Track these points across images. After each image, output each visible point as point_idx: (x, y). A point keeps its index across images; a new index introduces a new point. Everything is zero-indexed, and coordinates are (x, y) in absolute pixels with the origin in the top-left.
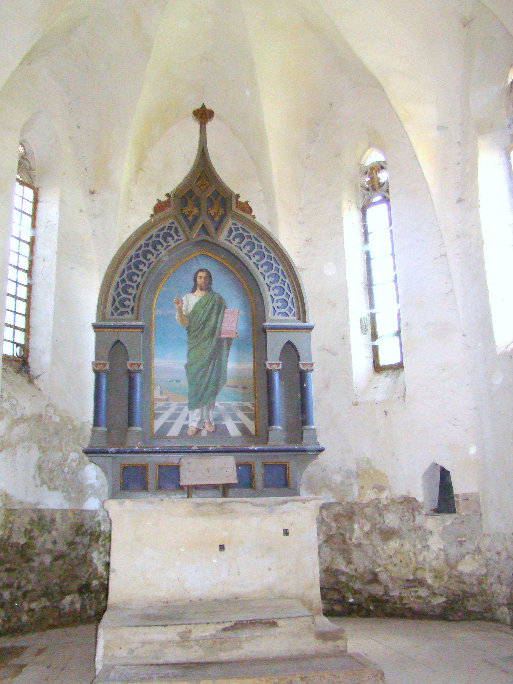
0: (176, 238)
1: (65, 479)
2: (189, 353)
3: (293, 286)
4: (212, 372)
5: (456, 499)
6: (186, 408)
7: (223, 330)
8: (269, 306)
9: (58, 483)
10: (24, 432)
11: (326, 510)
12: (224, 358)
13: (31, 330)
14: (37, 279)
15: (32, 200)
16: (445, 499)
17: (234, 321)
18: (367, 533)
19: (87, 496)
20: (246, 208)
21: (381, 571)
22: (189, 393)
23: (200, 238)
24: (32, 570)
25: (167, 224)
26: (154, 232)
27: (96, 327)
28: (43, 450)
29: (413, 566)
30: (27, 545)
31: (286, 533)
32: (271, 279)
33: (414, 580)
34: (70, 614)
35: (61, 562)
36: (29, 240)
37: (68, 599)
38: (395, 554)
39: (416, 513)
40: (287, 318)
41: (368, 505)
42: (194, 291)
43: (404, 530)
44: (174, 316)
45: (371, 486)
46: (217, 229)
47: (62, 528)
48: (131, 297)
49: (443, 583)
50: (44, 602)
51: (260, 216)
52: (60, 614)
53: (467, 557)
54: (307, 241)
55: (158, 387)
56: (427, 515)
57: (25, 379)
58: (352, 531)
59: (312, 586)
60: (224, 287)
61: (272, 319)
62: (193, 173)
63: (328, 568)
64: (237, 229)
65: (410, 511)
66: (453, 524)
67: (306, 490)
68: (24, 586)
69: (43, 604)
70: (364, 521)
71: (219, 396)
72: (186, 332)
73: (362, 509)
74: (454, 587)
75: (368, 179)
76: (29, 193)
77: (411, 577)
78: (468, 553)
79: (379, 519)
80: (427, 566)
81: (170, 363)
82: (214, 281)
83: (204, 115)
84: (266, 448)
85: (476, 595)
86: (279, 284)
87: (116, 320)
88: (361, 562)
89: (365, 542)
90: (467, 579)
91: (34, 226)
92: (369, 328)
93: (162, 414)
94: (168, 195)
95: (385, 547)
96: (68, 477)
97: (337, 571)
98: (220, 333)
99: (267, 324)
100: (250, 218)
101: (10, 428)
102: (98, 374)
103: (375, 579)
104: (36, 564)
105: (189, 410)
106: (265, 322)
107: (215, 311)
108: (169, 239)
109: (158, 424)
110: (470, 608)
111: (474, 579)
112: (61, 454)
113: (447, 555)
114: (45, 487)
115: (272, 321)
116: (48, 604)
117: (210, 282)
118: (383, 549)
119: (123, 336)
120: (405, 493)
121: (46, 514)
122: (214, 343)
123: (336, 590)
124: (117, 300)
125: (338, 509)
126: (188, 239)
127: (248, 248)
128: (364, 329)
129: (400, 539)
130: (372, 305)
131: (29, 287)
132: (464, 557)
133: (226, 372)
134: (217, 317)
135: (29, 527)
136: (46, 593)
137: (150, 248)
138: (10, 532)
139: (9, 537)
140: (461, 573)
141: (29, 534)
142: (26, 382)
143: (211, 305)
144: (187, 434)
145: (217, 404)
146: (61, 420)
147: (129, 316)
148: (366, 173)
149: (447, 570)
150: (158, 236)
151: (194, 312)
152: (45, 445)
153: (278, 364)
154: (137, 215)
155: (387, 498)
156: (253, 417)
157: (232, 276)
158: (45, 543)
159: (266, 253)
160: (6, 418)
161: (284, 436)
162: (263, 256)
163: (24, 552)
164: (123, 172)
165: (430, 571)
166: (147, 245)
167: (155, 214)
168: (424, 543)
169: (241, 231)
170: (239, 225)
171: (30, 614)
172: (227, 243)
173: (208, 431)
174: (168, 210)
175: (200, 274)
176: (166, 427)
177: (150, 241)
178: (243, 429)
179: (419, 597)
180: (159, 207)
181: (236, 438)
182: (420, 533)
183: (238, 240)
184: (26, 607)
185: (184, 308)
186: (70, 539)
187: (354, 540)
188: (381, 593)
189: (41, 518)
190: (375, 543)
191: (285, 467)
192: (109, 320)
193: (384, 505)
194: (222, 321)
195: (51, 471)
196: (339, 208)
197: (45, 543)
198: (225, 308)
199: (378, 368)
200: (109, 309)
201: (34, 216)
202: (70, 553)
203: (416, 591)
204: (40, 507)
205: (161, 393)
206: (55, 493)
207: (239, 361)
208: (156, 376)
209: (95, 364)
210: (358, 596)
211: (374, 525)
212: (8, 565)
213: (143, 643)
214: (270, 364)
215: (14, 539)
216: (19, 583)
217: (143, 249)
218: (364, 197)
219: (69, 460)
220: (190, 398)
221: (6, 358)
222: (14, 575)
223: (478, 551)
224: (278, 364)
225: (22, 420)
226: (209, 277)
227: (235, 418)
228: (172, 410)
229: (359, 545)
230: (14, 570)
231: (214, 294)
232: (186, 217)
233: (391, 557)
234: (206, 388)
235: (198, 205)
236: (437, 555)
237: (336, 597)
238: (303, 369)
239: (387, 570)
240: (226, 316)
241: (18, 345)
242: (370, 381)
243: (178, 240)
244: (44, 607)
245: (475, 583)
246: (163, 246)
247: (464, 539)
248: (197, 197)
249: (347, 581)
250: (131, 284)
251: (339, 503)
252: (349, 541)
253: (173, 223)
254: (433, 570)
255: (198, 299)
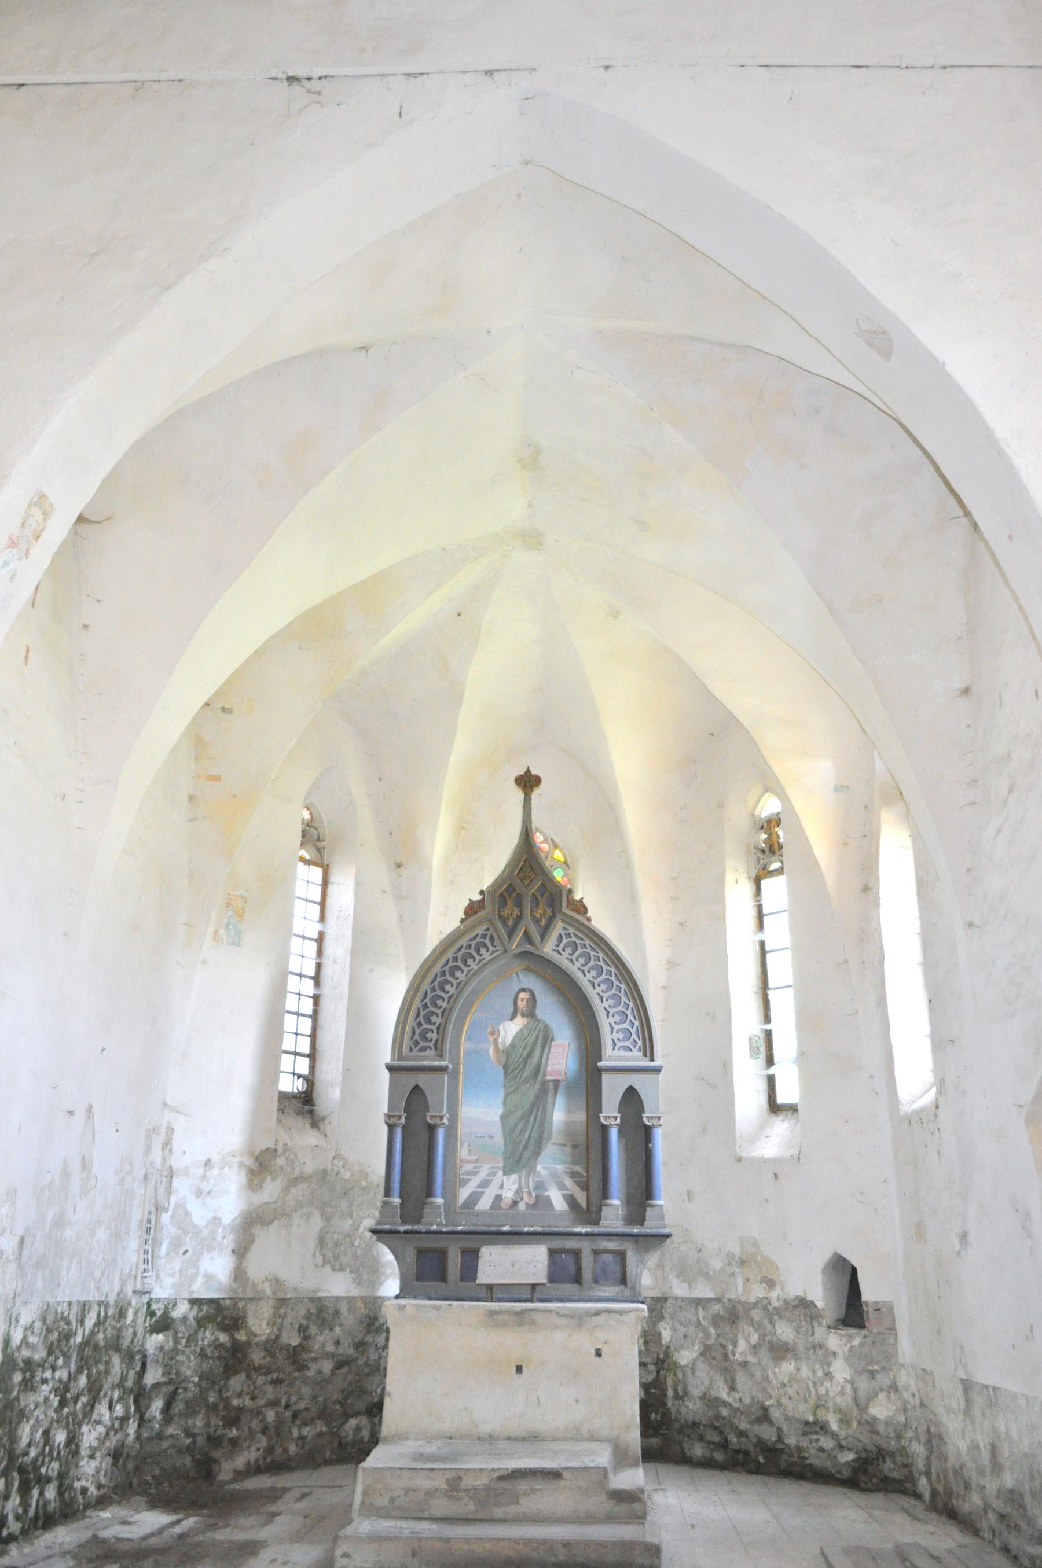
0: (491, 949)
1: (355, 1255)
2: (507, 1096)
3: (639, 1011)
4: (533, 1126)
5: (865, 1308)
6: (500, 1173)
7: (549, 1068)
8: (607, 1050)
9: (345, 1260)
10: (303, 1195)
11: (704, 1308)
12: (549, 1106)
13: (318, 1056)
14: (327, 990)
15: (320, 882)
16: (853, 1311)
17: (562, 1058)
18: (754, 1347)
19: (383, 1278)
20: (581, 908)
21: (772, 1405)
22: (505, 1153)
23: (521, 949)
24: (305, 1381)
25: (481, 930)
26: (464, 941)
27: (390, 1068)
28: (327, 1218)
29: (812, 1401)
30: (301, 1347)
31: (598, 1353)
32: (611, 1002)
33: (815, 1423)
34: (354, 1443)
35: (344, 1370)
36: (316, 936)
37: (353, 1422)
38: (789, 1381)
39: (816, 1324)
40: (629, 1054)
41: (755, 1305)
42: (513, 1017)
43: (801, 1348)
44: (487, 1051)
45: (759, 1278)
46: (543, 936)
47: (349, 1320)
48: (434, 1028)
49: (850, 1432)
50: (320, 1427)
51: (600, 919)
52: (340, 1443)
53: (882, 1396)
54: (681, 924)
55: (466, 1144)
56: (829, 1327)
57: (307, 1123)
58: (735, 1344)
59: (628, 1427)
60: (552, 1013)
61: (611, 1055)
62: (511, 865)
63: (705, 1394)
64: (569, 936)
65: (809, 1319)
66: (861, 1345)
67: (678, 1276)
68: (295, 1403)
69: (318, 1429)
70: (751, 1329)
71: (541, 1158)
72: (502, 1072)
73: (747, 1312)
74: (865, 1438)
75: (764, 836)
76: (317, 873)
77: (811, 1419)
78: (882, 1390)
79: (769, 1327)
80: (831, 1404)
81: (479, 1113)
82: (538, 1003)
83: (528, 782)
84: (596, 1230)
85: (893, 1453)
86: (620, 1008)
87: (414, 1059)
88: (746, 1392)
89: (751, 1359)
90: (881, 1428)
91: (322, 918)
92: (763, 1049)
93: (470, 1180)
94: (482, 892)
95: (777, 1370)
96: (359, 1252)
97: (717, 1399)
98: (545, 1074)
99: (600, 1064)
100: (585, 922)
101: (286, 1190)
102: (391, 1128)
103: (764, 1416)
104: (310, 1373)
105: (504, 1174)
106: (601, 1060)
107: (539, 1044)
108: (483, 951)
109: (464, 1194)
110: (887, 1473)
111: (890, 1429)
112: (351, 1222)
113: (855, 1390)
114: (328, 1268)
115: (610, 1059)
116: (324, 1429)
117: (534, 1007)
118: (774, 1373)
119: (423, 1080)
120: (801, 1294)
121: (328, 1304)
122: (537, 1087)
123: (716, 1428)
124: (418, 1031)
125: (717, 1308)
126: (506, 951)
127: (582, 961)
128: (754, 1052)
129: (797, 1359)
130: (767, 1019)
131: (316, 999)
132: (876, 1395)
133: (551, 1124)
134: (542, 1052)
135: (304, 1322)
136: (324, 1414)
137: (460, 964)
138: (280, 1329)
139: (278, 1337)
140: (875, 1419)
141: (304, 1332)
142: (308, 1126)
143: (534, 1036)
144: (501, 1208)
145: (539, 1168)
146: (352, 1175)
147: (431, 1053)
148: (762, 828)
149: (855, 1412)
150: (469, 947)
151: (513, 1045)
152: (329, 1210)
153: (616, 1118)
154: (442, 918)
155: (778, 1299)
156: (585, 1187)
157: (562, 999)
158: (323, 1345)
159: (605, 967)
160: (280, 1178)
161: (620, 1212)
162: (600, 972)
163: (297, 1357)
164: (439, 842)
165: (835, 1412)
166: (456, 959)
167: (466, 918)
168: (826, 1368)
169: (574, 939)
170: (571, 930)
171: (300, 1442)
172: (556, 954)
173: (527, 1204)
174: (482, 913)
175: (522, 995)
176: (474, 1198)
177: (460, 954)
178: (571, 1201)
179: (822, 1450)
180: (472, 909)
181: (561, 1215)
182: (820, 1353)
183: (569, 950)
184: (295, 1434)
185: (500, 1040)
186: (360, 1337)
187: (737, 1356)
188: (774, 1439)
189: (321, 1309)
190: (764, 1363)
191: (622, 1255)
192: (406, 1059)
193: (775, 1309)
194: (548, 1058)
195: (337, 1245)
196: (721, 881)
197: (323, 1345)
198: (553, 1040)
199: (774, 1107)
200: (407, 1043)
201: (323, 904)
202: (357, 1358)
203: (817, 1440)
204: (320, 1294)
205: (470, 1151)
206: (341, 1275)
207: (568, 1111)
208: (462, 1130)
209: (389, 1116)
210: (744, 1440)
211: (762, 1337)
212: (275, 1375)
213: (407, 1491)
214: (606, 1118)
215: (285, 1339)
216: (288, 1399)
217: (450, 964)
218: (759, 862)
219: (361, 1229)
220: (506, 1159)
221: (284, 1096)
222: (284, 1388)
223: (894, 1387)
224: (616, 1118)
225: (301, 1179)
226: (533, 999)
227: (562, 1187)
228: (482, 1177)
229: (745, 1364)
230: (282, 1382)
231: (538, 1021)
232: (504, 921)
233: (785, 1385)
234: (526, 1147)
235: (519, 904)
236: (842, 1387)
237: (716, 1439)
238: (647, 1123)
239: (780, 1404)
240: (553, 1050)
241: (299, 1076)
242: (763, 1126)
243: (494, 952)
244: (320, 1434)
245: (892, 1435)
246: (475, 960)
247: (876, 1367)
248: (518, 894)
249: (730, 1415)
250: (462, 966)
251: (718, 1300)
252: (731, 1357)
253: (488, 929)
254: (838, 1410)
255: (518, 1028)
